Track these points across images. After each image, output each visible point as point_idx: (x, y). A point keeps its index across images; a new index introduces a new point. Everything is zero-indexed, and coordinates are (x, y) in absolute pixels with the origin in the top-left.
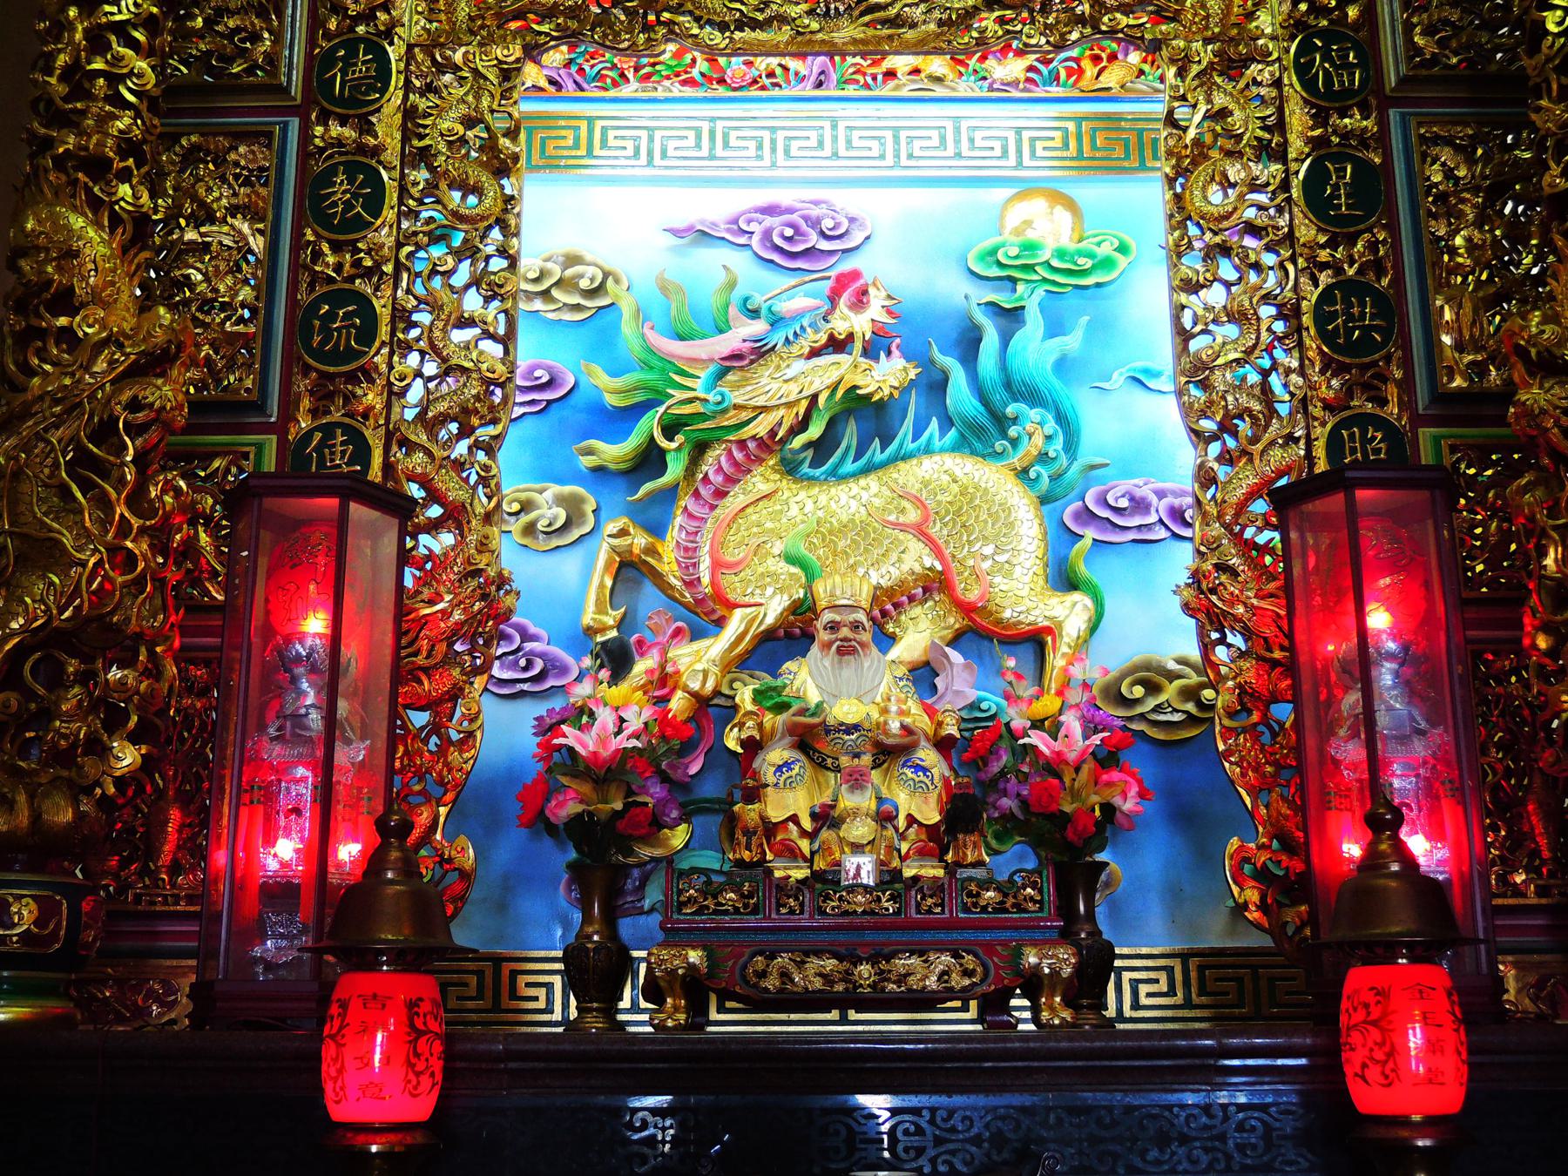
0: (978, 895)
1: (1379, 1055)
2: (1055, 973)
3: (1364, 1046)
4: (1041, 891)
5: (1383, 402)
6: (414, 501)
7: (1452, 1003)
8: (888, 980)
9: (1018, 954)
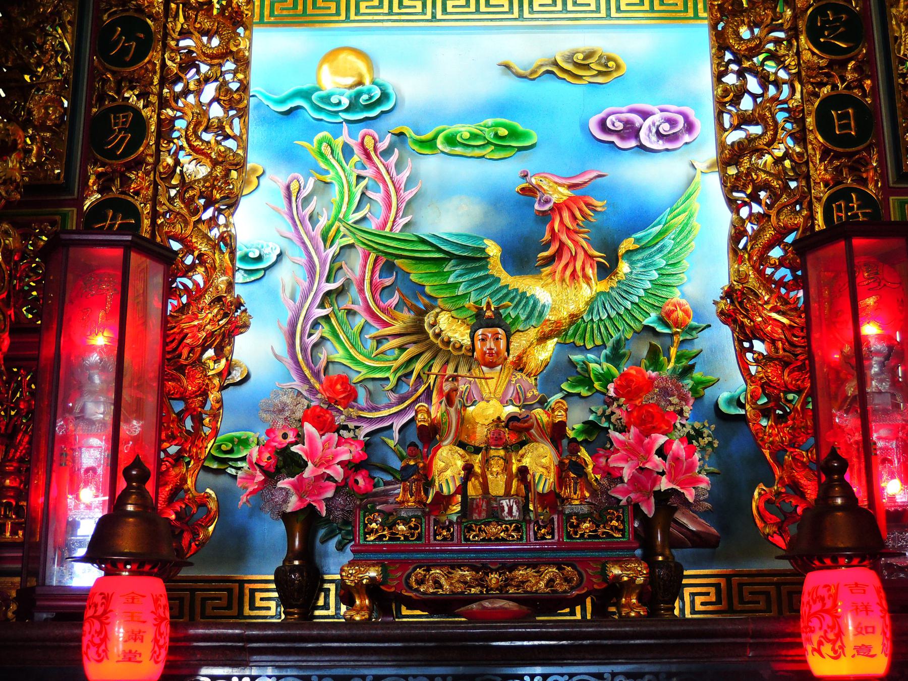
0: (578, 526)
1: (97, 640)
2: (632, 580)
3: (90, 633)
4: (623, 522)
5: (864, 182)
6: (176, 253)
7: (880, 598)
8: (511, 585)
9: (604, 569)
